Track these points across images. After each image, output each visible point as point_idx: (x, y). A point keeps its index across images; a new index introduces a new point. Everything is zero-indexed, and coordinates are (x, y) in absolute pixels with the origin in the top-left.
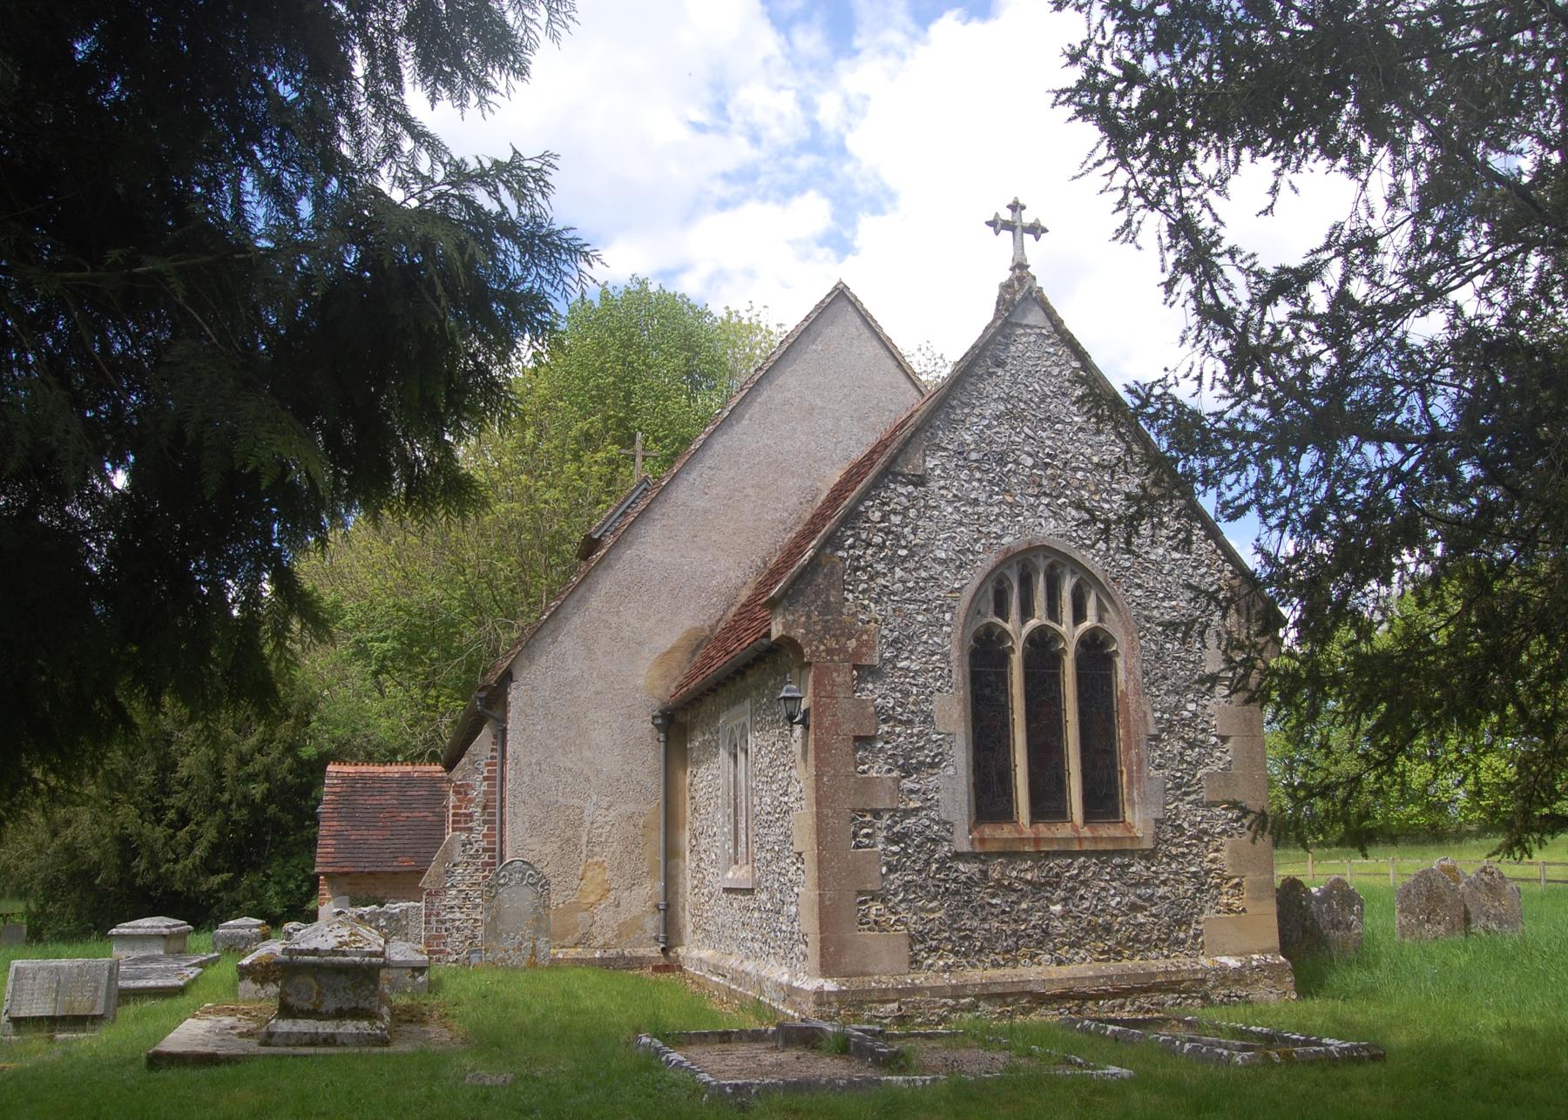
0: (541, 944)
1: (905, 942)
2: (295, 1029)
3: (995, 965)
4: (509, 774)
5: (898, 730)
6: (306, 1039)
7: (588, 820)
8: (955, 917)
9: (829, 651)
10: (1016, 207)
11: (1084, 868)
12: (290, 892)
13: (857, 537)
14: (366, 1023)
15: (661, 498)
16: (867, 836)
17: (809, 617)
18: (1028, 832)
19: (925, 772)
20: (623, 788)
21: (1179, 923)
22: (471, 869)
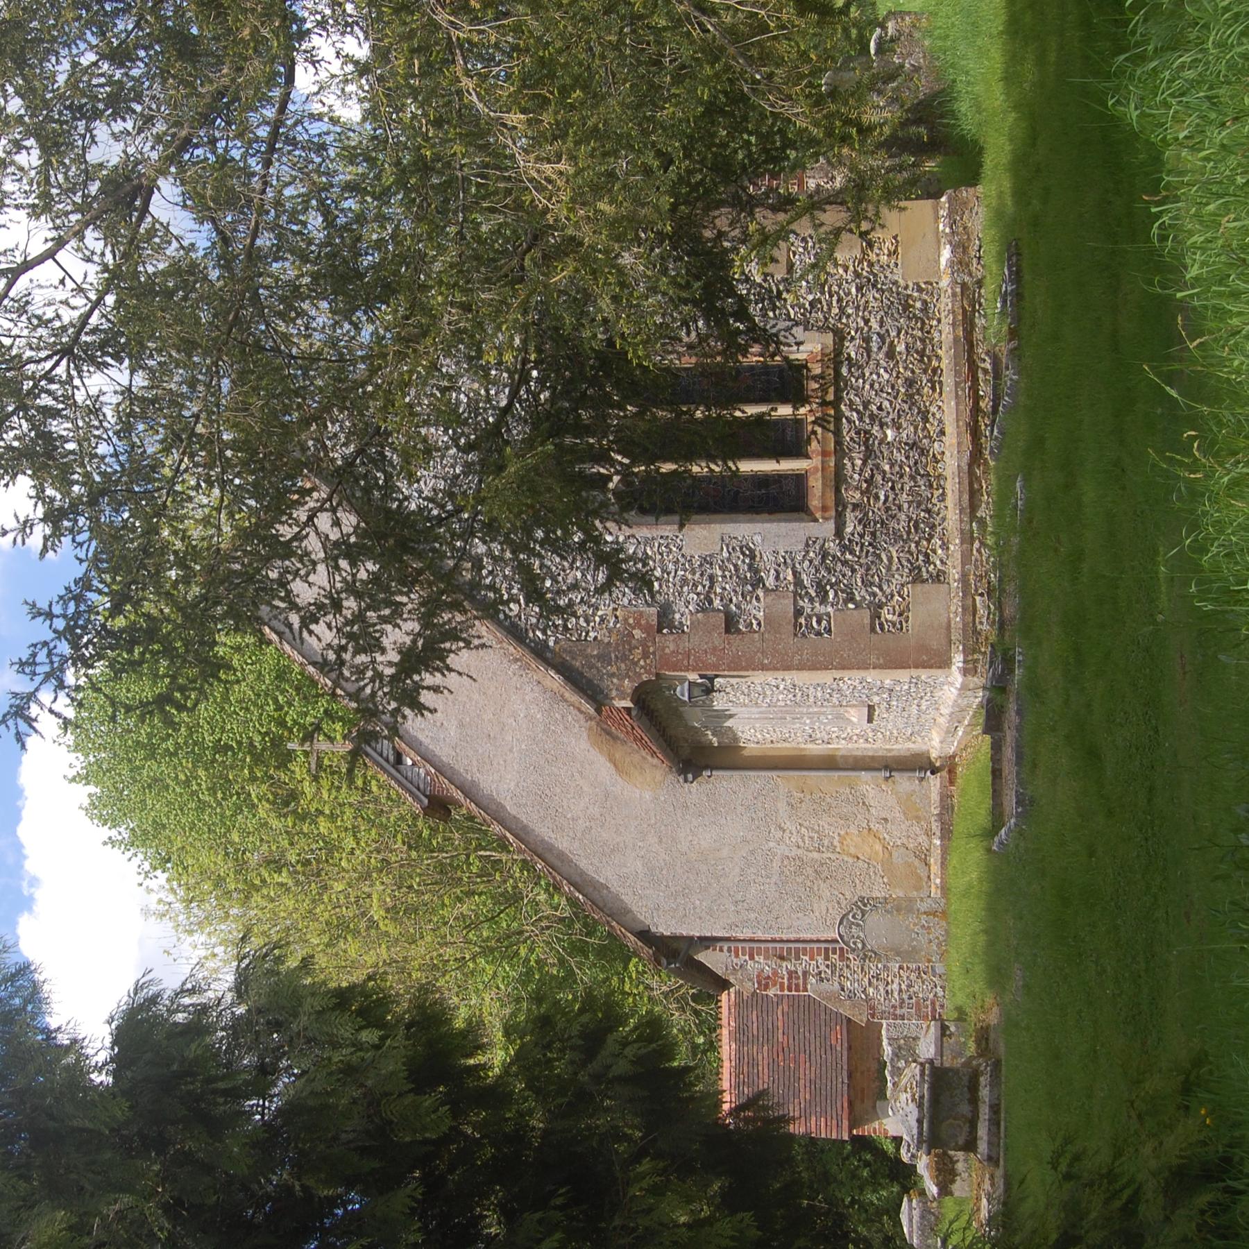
0: (924, 907)
1: (919, 587)
2: (985, 1138)
3: (943, 498)
4: (748, 934)
6: (994, 1129)
7: (795, 852)
8: (897, 537)
9: (645, 655)
11: (851, 405)
12: (873, 1175)
14: (982, 1079)
15: (449, 774)
16: (819, 622)
17: (613, 675)
18: (816, 461)
19: (758, 563)
20: (761, 814)
21: (907, 307)
22: (846, 972)
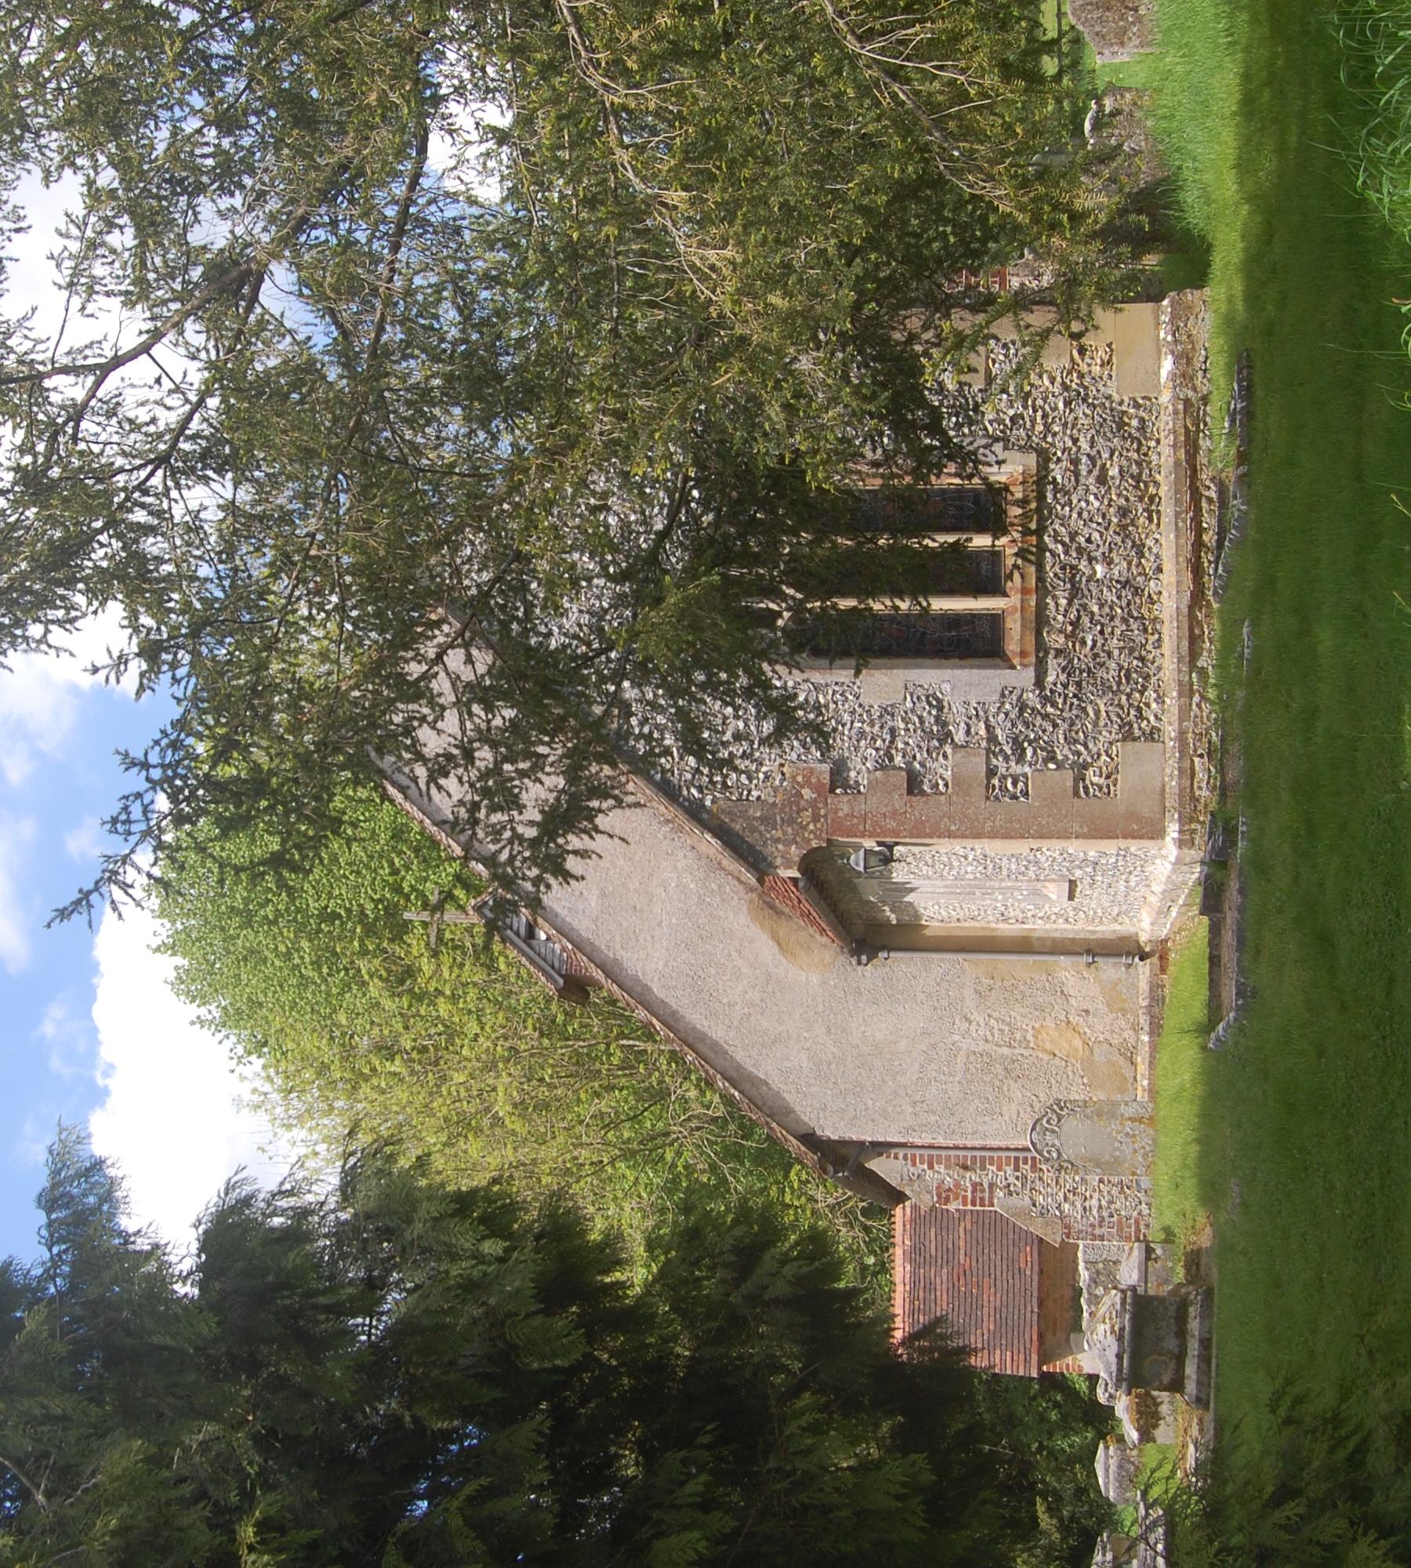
0: (1129, 1112)
1: (1130, 745)
3: (1158, 644)
4: (926, 1140)
5: (900, 746)
6: (1203, 1367)
7: (982, 1047)
8: (1106, 688)
9: (815, 818)
11: (1056, 537)
12: (1064, 1418)
13: (689, 784)
15: (588, 950)
16: (1015, 784)
17: (778, 840)
20: (945, 1003)
21: (1121, 425)
22: (1039, 1185)
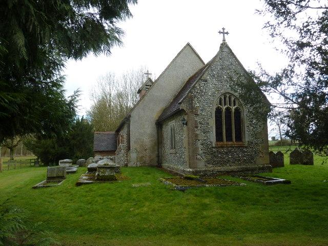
10: (223, 29)
